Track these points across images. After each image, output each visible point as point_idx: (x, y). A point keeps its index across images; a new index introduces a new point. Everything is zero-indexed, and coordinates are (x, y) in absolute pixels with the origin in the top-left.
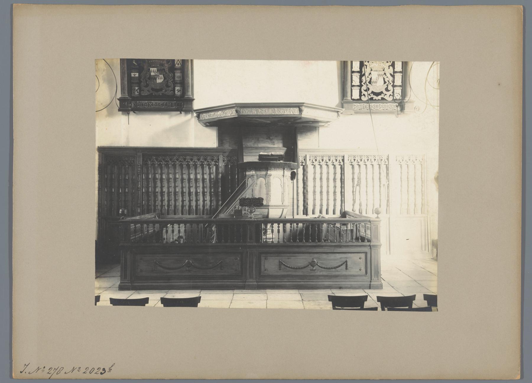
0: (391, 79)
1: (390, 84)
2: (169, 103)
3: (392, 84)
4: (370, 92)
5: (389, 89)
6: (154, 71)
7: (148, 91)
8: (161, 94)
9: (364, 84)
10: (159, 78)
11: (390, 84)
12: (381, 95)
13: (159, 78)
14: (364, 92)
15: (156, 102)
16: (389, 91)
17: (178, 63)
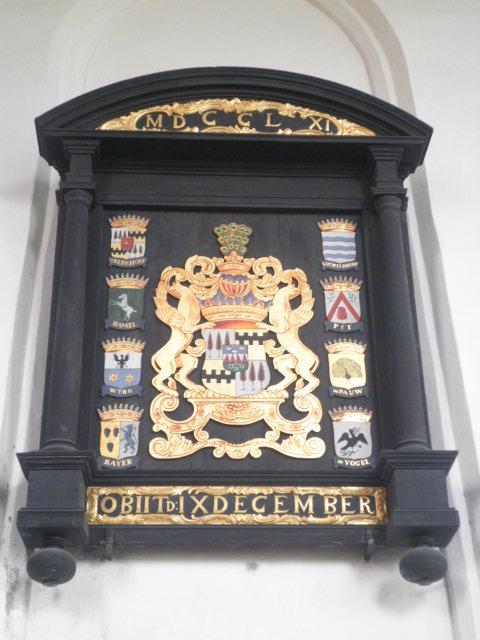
0: (307, 359)
1: (306, 382)
2: (304, 499)
3: (314, 382)
4: (196, 423)
5: (298, 404)
6: (223, 342)
7: (190, 436)
8: (257, 454)
9: (166, 382)
10: (248, 373)
11: (306, 382)
12: (263, 437)
13: (248, 373)
14: (162, 424)
15: (231, 489)
16: (303, 415)
17: (342, 310)
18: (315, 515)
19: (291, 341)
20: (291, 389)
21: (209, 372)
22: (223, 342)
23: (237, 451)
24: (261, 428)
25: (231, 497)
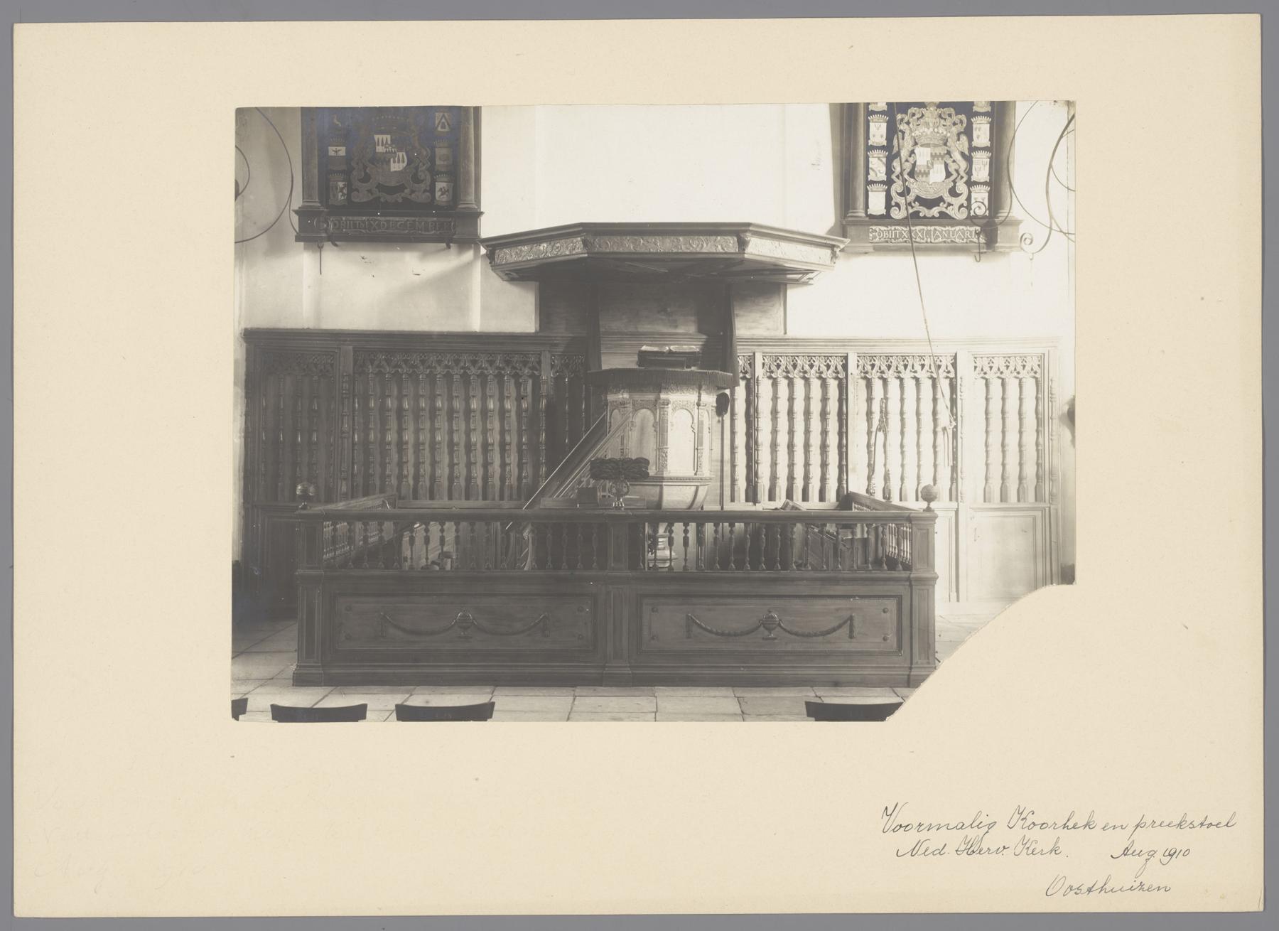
0: (963, 165)
4: (911, 198)
6: (384, 142)
7: (369, 191)
8: (400, 200)
9: (898, 177)
10: (396, 159)
11: (962, 178)
13: (396, 159)
18: (425, 231)
19: (957, 156)
20: (954, 182)
21: (918, 171)
22: (384, 142)
23: (389, 198)
24: (941, 199)
25: (388, 222)
